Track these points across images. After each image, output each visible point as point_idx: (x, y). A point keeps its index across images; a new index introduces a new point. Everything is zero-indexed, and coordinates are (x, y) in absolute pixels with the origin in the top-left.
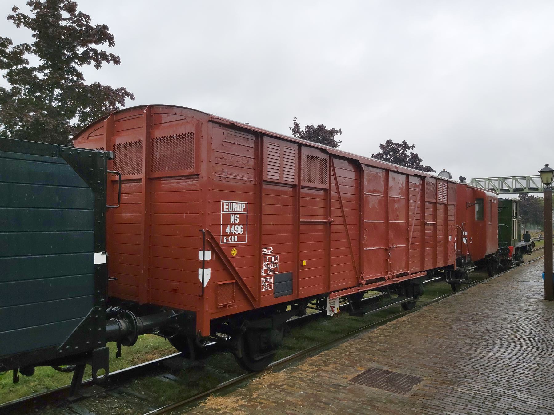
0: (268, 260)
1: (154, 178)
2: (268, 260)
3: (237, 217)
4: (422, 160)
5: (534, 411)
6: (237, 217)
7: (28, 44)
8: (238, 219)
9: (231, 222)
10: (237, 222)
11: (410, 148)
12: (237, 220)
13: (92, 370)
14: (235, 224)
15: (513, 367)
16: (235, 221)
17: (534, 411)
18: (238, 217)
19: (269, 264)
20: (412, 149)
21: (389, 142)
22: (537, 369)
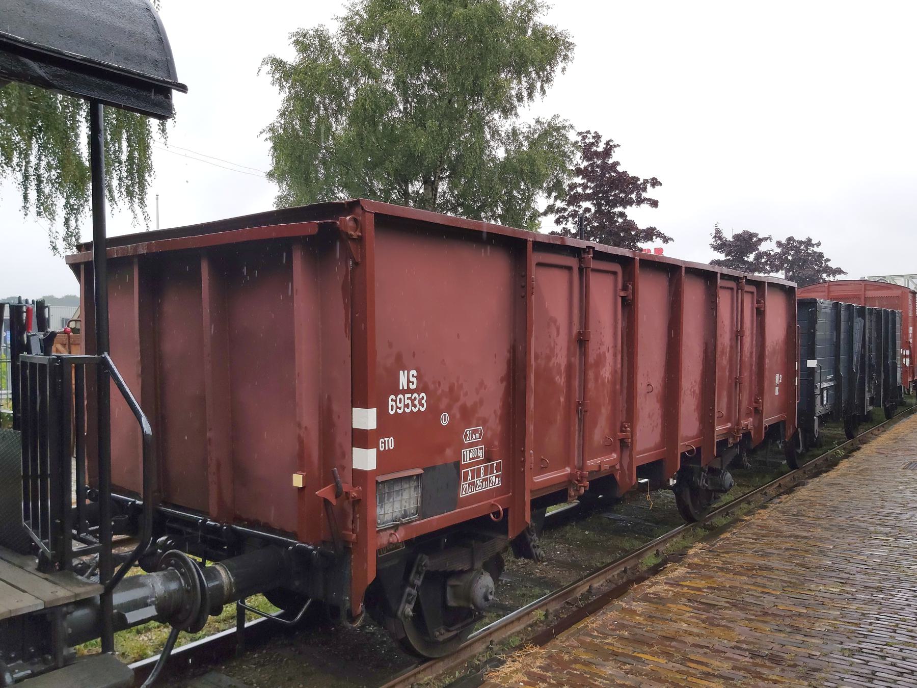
0: (470, 477)
1: (587, 287)
2: (470, 477)
3: (413, 375)
4: (661, 184)
5: (869, 664)
6: (413, 375)
7: (740, 232)
8: (414, 380)
9: (401, 388)
10: (413, 387)
11: (815, 246)
12: (413, 383)
13: (179, 636)
14: (409, 391)
15: (863, 636)
16: (411, 384)
17: (869, 664)
18: (415, 375)
19: (472, 484)
20: (818, 246)
21: (790, 239)
22: (892, 665)
